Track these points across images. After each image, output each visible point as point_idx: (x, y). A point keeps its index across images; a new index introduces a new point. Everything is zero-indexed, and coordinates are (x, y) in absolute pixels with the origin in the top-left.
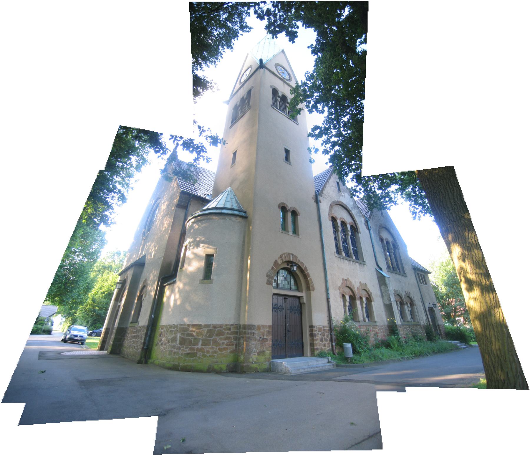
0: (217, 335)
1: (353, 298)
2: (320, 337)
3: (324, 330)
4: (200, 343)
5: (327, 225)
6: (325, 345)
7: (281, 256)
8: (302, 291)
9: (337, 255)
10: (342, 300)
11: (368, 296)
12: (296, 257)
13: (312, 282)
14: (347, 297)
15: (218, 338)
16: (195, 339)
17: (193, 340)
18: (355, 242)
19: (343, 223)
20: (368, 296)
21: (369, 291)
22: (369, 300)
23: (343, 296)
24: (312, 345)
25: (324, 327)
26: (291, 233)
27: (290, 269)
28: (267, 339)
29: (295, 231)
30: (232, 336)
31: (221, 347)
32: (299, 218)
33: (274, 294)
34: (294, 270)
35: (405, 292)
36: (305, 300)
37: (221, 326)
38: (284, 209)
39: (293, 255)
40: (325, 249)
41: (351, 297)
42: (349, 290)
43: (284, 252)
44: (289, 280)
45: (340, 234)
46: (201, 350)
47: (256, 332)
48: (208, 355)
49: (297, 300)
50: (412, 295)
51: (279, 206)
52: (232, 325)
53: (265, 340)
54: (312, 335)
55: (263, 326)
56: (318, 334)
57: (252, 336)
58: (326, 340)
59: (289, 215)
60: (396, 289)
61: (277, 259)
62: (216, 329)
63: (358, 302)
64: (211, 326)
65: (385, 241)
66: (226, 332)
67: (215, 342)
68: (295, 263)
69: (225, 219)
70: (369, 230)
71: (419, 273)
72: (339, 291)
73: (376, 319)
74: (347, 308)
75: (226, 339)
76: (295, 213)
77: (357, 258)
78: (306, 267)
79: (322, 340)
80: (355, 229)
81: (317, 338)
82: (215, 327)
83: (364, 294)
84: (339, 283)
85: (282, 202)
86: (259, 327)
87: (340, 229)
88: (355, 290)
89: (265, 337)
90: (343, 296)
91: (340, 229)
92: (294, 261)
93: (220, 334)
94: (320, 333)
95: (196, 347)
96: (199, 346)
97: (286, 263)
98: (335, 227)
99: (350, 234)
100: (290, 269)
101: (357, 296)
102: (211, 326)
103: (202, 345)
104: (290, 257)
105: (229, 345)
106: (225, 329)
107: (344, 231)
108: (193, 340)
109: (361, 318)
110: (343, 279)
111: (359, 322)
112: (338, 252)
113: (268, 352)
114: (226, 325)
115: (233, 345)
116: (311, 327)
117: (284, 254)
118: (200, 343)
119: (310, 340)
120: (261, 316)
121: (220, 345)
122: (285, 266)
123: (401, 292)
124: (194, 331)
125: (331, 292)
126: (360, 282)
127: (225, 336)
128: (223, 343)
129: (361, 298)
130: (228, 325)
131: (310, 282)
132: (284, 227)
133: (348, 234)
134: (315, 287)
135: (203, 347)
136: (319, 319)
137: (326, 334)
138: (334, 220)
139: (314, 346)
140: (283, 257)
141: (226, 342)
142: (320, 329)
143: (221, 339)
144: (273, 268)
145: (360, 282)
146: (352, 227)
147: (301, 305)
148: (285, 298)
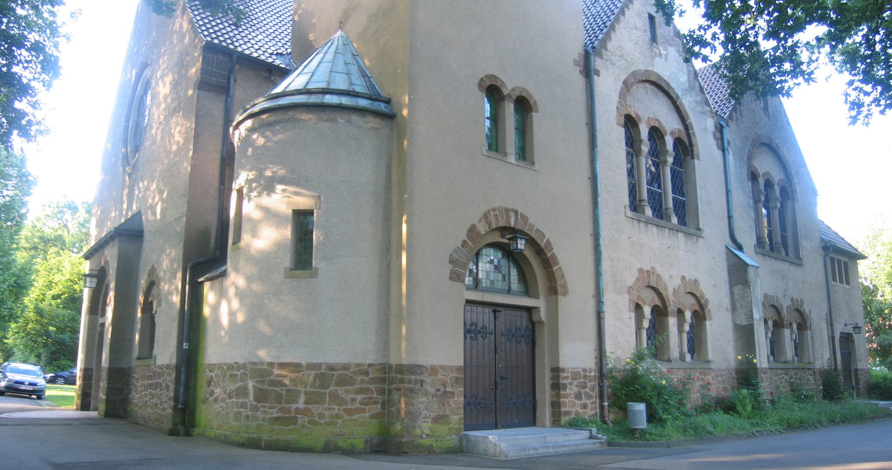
0: (338, 384)
1: (660, 312)
2: (576, 389)
3: (585, 377)
5: (613, 138)
6: (585, 406)
7: (486, 216)
8: (536, 297)
9: (629, 213)
10: (633, 315)
11: (697, 308)
12: (525, 219)
13: (563, 276)
14: (647, 311)
15: (341, 391)
16: (288, 391)
17: (284, 393)
18: (682, 182)
19: (656, 133)
20: (697, 308)
21: (703, 296)
22: (700, 315)
23: (638, 307)
24: (556, 405)
25: (585, 370)
26: (512, 159)
27: (508, 245)
28: (453, 394)
29: (524, 153)
30: (372, 387)
31: (349, 407)
32: (537, 119)
33: (469, 302)
35: (792, 299)
36: (543, 315)
37: (346, 367)
38: (493, 91)
39: (516, 212)
42: (653, 294)
43: (493, 206)
44: (505, 270)
46: (305, 412)
47: (428, 380)
48: (322, 421)
50: (806, 308)
51: (480, 85)
52: (370, 365)
54: (556, 386)
55: (443, 368)
57: (418, 386)
58: (589, 396)
59: (509, 108)
60: (770, 293)
61: (475, 221)
62: (336, 373)
63: (672, 321)
64: (324, 367)
65: (761, 181)
66: (359, 378)
67: (335, 397)
68: (523, 233)
69: (334, 120)
70: (723, 150)
71: (837, 257)
73: (710, 356)
74: (685, 336)
75: (360, 391)
76: (524, 105)
77: (682, 221)
79: (578, 396)
80: (685, 148)
81: (568, 391)
82: (331, 368)
83: (794, 318)
84: (630, 279)
86: (434, 370)
87: (645, 148)
88: (669, 294)
89: (449, 389)
90: (638, 307)
91: (645, 148)
93: (344, 381)
94: (575, 382)
95: (294, 406)
96: (301, 404)
98: (632, 142)
99: (670, 160)
100: (508, 245)
101: (672, 308)
102: (324, 367)
103: (306, 403)
104: (508, 218)
105: (368, 404)
107: (657, 152)
108: (284, 393)
109: (675, 353)
110: (640, 270)
111: (670, 361)
112: (635, 206)
113: (456, 417)
114: (358, 365)
115: (376, 403)
116: (556, 371)
117: (494, 210)
118: (302, 398)
120: (440, 346)
121: (347, 403)
123: (782, 300)
124: (285, 376)
126: (683, 278)
127: (357, 386)
128: (353, 400)
129: (680, 312)
130: (363, 364)
131: (557, 275)
132: (495, 144)
133: (665, 162)
135: (310, 406)
136: (575, 354)
137: (589, 385)
139: (559, 407)
140: (493, 219)
141: (359, 397)
142: (575, 375)
143: (347, 391)
145: (683, 278)
146: (678, 142)
147: (533, 325)
148: (494, 311)
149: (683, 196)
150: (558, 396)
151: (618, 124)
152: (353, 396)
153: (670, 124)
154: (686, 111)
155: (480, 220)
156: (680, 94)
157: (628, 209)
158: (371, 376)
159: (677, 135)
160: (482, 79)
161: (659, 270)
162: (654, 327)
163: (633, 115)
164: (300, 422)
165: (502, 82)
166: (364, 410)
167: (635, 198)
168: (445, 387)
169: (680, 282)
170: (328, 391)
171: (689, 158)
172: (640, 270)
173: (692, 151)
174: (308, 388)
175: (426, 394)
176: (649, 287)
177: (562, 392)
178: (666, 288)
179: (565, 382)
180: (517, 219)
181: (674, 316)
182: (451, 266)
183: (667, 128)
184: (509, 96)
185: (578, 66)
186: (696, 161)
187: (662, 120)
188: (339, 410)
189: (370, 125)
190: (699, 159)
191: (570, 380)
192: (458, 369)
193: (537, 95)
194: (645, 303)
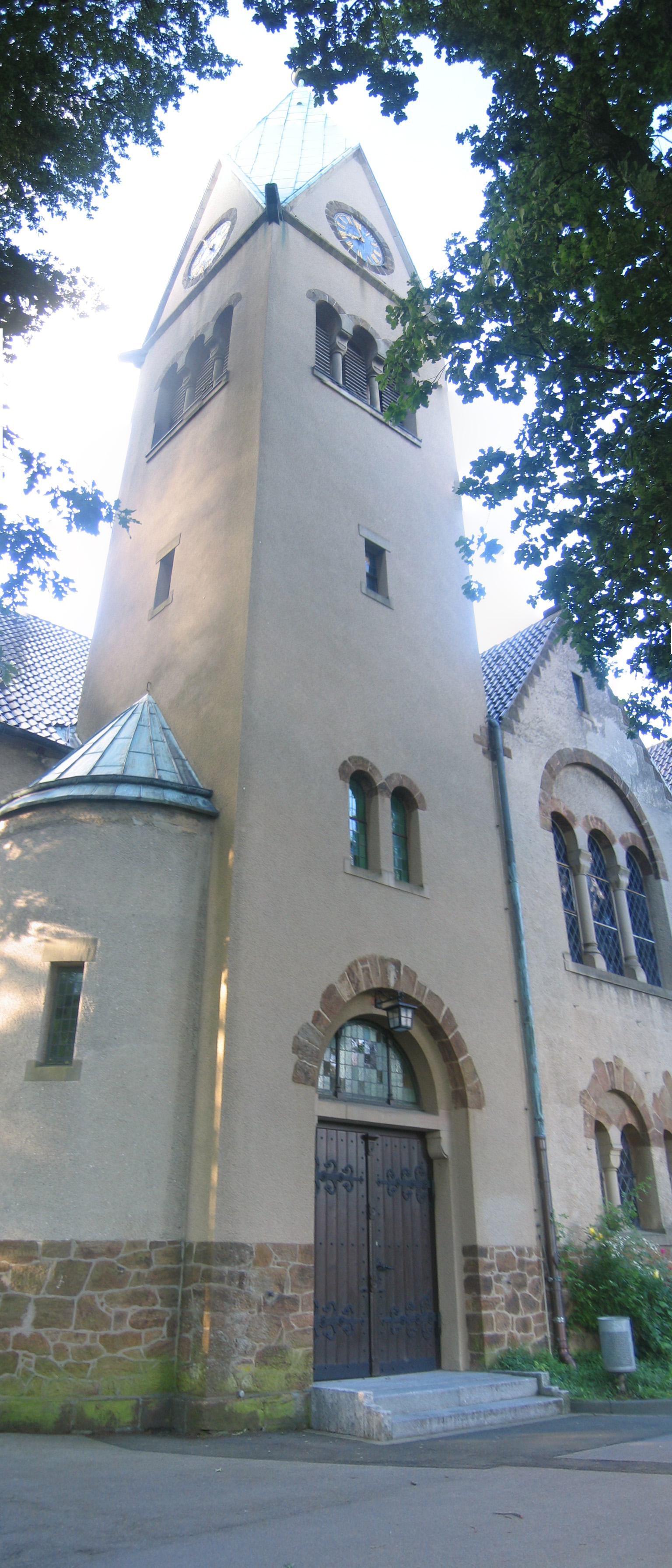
0: (97, 1284)
1: (636, 1138)
2: (507, 1290)
3: (522, 1264)
4: (30, 1316)
5: (536, 848)
6: (524, 1325)
7: (350, 972)
8: (434, 1111)
9: (572, 966)
10: (592, 1144)
12: (411, 975)
13: (475, 1073)
14: (615, 1134)
15: (99, 1298)
19: (599, 840)
23: (600, 1129)
24: (475, 1323)
25: (520, 1251)
28: (294, 1301)
29: (408, 870)
30: (155, 1288)
31: (112, 1332)
33: (324, 1121)
34: (404, 1028)
36: (445, 1144)
37: (112, 1249)
38: (361, 781)
39: (397, 964)
40: (524, 943)
41: (628, 1133)
45: (584, 880)
46: (32, 1344)
47: (253, 1273)
48: (61, 1363)
49: (415, 1143)
52: (154, 1245)
53: (285, 1304)
54: (474, 1284)
56: (498, 1279)
58: (531, 1305)
59: (384, 806)
62: (94, 1261)
64: (74, 1248)
66: (133, 1271)
67: (88, 1311)
68: (407, 998)
69: (128, 822)
72: (580, 1109)
74: (614, 1177)
75: (135, 1298)
76: (405, 800)
78: (449, 1015)
79: (512, 1305)
81: (494, 1294)
82: (87, 1251)
84: (583, 1078)
85: (356, 753)
86: (263, 1254)
87: (586, 862)
88: (647, 1103)
89: (288, 1293)
90: (600, 1129)
91: (586, 862)
92: (403, 988)
93: (108, 1279)
94: (506, 1276)
95: (14, 1331)
97: (370, 999)
98: (565, 853)
99: (625, 880)
100: (386, 1019)
103: (37, 1324)
104: (386, 973)
105: (145, 1325)
106: (126, 1261)
107: (604, 869)
110: (597, 1062)
112: (579, 953)
114: (134, 1245)
115: (159, 1322)
116: (472, 1251)
117: (363, 961)
118: (30, 1316)
119: (467, 1305)
120: (273, 1208)
121: (108, 1326)
122: (368, 1008)
125: (550, 1112)
127: (128, 1288)
130: (141, 1243)
131: (466, 1072)
132: (364, 856)
133: (618, 883)
134: (488, 1091)
135: (42, 1331)
136: (502, 1221)
137: (530, 1280)
138: (560, 825)
139: (481, 1328)
140: (361, 975)
141: (131, 1311)
142: (505, 1262)
143: (111, 1299)
144: (317, 1017)
146: (633, 853)
147: (430, 1164)
148: (366, 1138)
149: (650, 936)
150: (477, 1303)
151: (543, 826)
152: (120, 1309)
153: (619, 826)
154: (639, 807)
155: (342, 977)
156: (628, 783)
157: (569, 959)
158: (155, 1266)
159: (631, 843)
160: (344, 764)
161: (626, 1062)
162: (629, 1165)
163: (563, 812)
164: (21, 1365)
165: (374, 768)
166: (137, 1339)
167: (577, 940)
168: (281, 1287)
169: (661, 1083)
170: (76, 1299)
171: (652, 877)
172: (597, 1062)
173: (656, 866)
174: (43, 1294)
175: (248, 1303)
176: (614, 1091)
177: (484, 1296)
178: (641, 1094)
179: (488, 1274)
180: (398, 975)
181: (659, 1145)
182: (295, 1057)
183: (614, 832)
184: (383, 787)
185: (481, 743)
186: (663, 882)
187: (606, 820)
188: (93, 1337)
189: (180, 829)
190: (666, 879)
191: (496, 1272)
192: (305, 1250)
193: (424, 786)
194: (610, 1121)
